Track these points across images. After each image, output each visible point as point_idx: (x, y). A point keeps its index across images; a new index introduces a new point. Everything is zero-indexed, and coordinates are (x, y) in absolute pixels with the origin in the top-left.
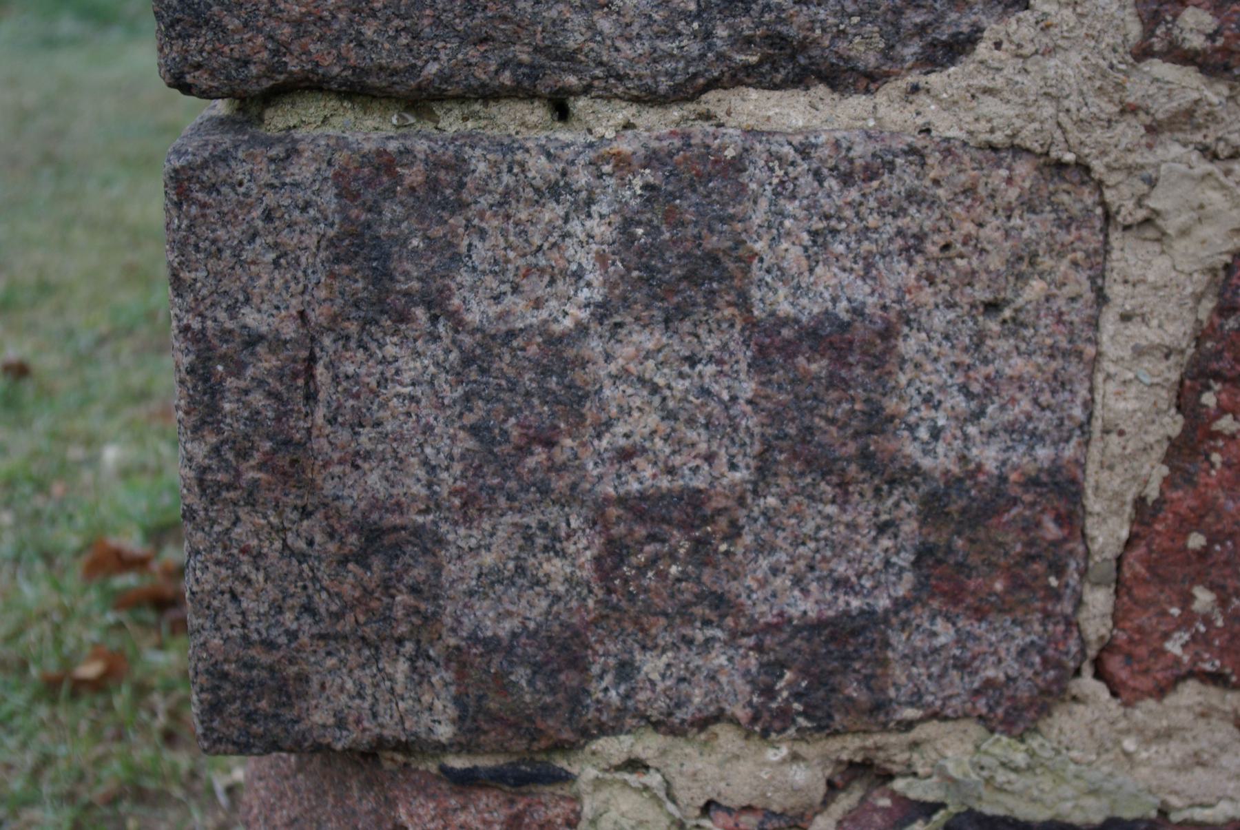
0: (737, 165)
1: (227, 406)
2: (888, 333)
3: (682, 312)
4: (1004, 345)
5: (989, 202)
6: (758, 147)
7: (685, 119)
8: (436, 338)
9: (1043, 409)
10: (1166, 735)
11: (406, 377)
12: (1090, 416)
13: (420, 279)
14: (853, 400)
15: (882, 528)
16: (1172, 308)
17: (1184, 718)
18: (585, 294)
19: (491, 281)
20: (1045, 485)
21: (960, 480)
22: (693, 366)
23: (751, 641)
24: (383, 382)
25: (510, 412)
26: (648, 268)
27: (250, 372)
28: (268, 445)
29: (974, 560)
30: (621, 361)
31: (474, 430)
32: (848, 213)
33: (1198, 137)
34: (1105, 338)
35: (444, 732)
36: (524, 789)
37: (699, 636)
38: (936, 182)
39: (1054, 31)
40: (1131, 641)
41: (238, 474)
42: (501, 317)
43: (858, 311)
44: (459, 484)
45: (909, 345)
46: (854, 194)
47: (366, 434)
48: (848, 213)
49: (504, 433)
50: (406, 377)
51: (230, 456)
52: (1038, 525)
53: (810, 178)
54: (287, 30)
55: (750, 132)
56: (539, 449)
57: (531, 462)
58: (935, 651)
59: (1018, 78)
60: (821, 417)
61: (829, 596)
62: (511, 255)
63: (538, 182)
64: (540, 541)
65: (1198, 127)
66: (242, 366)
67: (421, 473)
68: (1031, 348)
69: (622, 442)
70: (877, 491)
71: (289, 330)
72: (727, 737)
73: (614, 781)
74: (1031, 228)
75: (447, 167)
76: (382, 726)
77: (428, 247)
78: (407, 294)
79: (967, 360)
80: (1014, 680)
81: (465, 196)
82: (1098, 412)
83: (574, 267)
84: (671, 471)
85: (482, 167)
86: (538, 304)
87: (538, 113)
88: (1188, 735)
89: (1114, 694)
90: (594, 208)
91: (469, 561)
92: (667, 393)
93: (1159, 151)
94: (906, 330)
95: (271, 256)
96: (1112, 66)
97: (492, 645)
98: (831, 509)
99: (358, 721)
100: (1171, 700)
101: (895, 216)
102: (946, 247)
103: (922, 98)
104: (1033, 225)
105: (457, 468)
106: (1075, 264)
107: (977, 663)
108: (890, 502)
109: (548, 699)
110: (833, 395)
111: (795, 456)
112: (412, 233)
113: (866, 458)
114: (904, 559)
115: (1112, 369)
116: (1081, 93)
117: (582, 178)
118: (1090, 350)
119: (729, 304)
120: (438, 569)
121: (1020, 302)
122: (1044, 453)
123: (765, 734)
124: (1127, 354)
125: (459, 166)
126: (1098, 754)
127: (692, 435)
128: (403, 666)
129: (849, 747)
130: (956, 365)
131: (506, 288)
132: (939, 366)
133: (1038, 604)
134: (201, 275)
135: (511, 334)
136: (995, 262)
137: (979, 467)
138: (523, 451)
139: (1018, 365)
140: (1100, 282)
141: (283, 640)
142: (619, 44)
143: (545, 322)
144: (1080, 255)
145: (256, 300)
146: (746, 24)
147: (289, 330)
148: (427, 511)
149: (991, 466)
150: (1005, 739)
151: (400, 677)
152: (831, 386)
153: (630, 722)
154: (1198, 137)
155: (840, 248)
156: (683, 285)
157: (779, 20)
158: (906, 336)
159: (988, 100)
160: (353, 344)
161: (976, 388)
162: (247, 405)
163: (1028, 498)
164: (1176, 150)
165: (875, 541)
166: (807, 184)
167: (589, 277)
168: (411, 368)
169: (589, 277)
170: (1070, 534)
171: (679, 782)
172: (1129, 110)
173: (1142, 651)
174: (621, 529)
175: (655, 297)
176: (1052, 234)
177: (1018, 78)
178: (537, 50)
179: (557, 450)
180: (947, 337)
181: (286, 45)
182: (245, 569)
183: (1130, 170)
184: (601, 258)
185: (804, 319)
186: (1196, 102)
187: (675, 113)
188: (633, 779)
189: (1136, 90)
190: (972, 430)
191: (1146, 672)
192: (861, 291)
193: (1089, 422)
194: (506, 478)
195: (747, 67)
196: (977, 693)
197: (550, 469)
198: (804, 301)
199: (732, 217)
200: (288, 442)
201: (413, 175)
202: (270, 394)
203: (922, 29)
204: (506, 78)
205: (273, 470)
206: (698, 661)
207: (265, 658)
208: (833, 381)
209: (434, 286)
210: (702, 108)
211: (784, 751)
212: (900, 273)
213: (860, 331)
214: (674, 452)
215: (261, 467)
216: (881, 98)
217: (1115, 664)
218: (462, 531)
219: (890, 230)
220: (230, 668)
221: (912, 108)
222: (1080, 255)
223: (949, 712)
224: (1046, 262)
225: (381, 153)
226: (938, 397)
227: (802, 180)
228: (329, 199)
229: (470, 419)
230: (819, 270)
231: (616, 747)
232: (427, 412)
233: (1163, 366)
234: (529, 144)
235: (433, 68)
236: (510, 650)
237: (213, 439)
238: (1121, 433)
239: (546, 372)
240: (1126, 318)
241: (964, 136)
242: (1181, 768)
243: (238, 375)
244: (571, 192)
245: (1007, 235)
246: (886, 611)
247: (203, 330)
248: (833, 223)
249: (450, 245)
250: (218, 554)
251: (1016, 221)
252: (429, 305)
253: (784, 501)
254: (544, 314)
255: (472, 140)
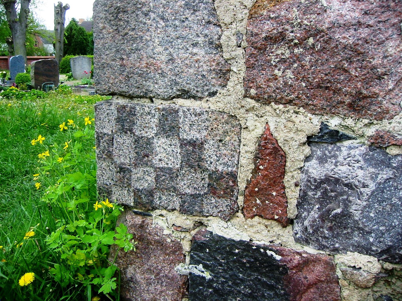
0: (177, 112)
1: (101, 144)
2: (202, 143)
3: (169, 136)
4: (223, 148)
5: (220, 121)
6: (181, 109)
7: (171, 103)
8: (131, 137)
9: (230, 161)
10: (252, 226)
11: (127, 143)
12: (238, 163)
13: (128, 126)
14: (196, 155)
15: (203, 179)
16: (251, 144)
17: (255, 223)
18: (154, 132)
19: (140, 128)
20: (229, 175)
21: (215, 172)
22: (171, 146)
23: (180, 196)
24: (123, 143)
25: (142, 150)
26: (163, 128)
27: (104, 139)
28: (107, 152)
29: (218, 187)
30: (159, 144)
31: (136, 153)
32: (196, 121)
33: (255, 113)
34: (241, 149)
35: (132, 204)
36: (145, 217)
37: (172, 194)
38: (210, 117)
39: (230, 91)
40: (247, 207)
41: (103, 156)
42: (141, 134)
43: (197, 139)
44: (134, 162)
45: (206, 146)
46: (197, 118)
47: (121, 151)
48: (196, 121)
49: (141, 154)
50: (127, 143)
51: (101, 152)
52: (229, 182)
53: (189, 114)
54: (110, 84)
55: (180, 106)
56: (146, 157)
57: (145, 159)
58: (211, 203)
59: (223, 100)
60: (191, 157)
61: (193, 190)
62: (143, 124)
63: (146, 112)
64: (146, 173)
65: (255, 111)
66: (103, 138)
67: (129, 159)
68: (228, 149)
69: (159, 158)
70: (201, 172)
71: (110, 133)
72: (176, 213)
73: (158, 218)
74: (227, 127)
75: (133, 108)
76: (123, 201)
77: (130, 121)
78: (127, 129)
79: (216, 150)
80: (225, 211)
81: (136, 113)
82: (240, 163)
83: (152, 127)
84: (167, 164)
85: (138, 109)
86: (147, 133)
87: (147, 100)
88: (256, 227)
89: (244, 216)
90: (155, 117)
91: (136, 175)
92: (166, 150)
93: (248, 115)
94: (206, 143)
95: (108, 121)
96: (239, 99)
97: (139, 190)
98: (194, 175)
99: (120, 200)
100: (253, 219)
101: (204, 123)
102: (212, 129)
103: (209, 102)
104: (227, 126)
105: (134, 159)
106: (235, 134)
107: (219, 207)
108: (204, 174)
109: (147, 201)
110: (193, 154)
111: (187, 164)
112: (127, 119)
113: (199, 166)
114: (206, 185)
115: (242, 155)
116: (234, 103)
117: (153, 112)
118: (238, 151)
119: (176, 136)
120: (131, 176)
121: (225, 140)
122: (230, 169)
123: (182, 213)
124: (244, 152)
125: (134, 108)
126: (240, 227)
127: (171, 158)
128: (126, 192)
129: (197, 218)
130: (215, 151)
131: (142, 129)
132: (212, 150)
133: (229, 197)
134: (98, 123)
135: (142, 137)
136: (220, 132)
137: (218, 170)
138: (144, 157)
139: (225, 152)
140: (240, 138)
141: (109, 184)
142: (158, 89)
143: (147, 136)
144: (235, 133)
145: (106, 128)
146: (178, 88)
147: (110, 133)
148: (129, 166)
149: (220, 170)
150: (223, 222)
151: (126, 193)
152: (192, 152)
153: (161, 208)
154: (255, 113)
155: (195, 128)
156: (169, 131)
157: (183, 87)
158: (206, 144)
159: (218, 103)
160: (119, 136)
161: (218, 155)
162: (104, 145)
163: (227, 177)
164: (251, 115)
165: (201, 181)
166: (189, 116)
167: (154, 129)
168: (128, 141)
169: (154, 129)
170: (235, 185)
171: (169, 220)
172: (242, 107)
173: (249, 209)
174: (159, 173)
175: (164, 133)
176: (231, 128)
177: (223, 100)
178: (146, 90)
179: (149, 158)
180: (213, 145)
181: (110, 87)
182: (103, 172)
183: (244, 118)
184: (156, 125)
185: (188, 139)
186: (254, 106)
187: (169, 102)
188: (161, 218)
189: (243, 103)
190: (217, 163)
191: (249, 213)
192: (198, 136)
193: (238, 164)
194: (141, 162)
195: (179, 95)
196: (219, 212)
197: (148, 161)
198: (188, 136)
199: (176, 120)
200: (109, 151)
201: (128, 109)
202: (107, 143)
203: (208, 90)
204: (142, 94)
205: (107, 156)
206: (171, 199)
207: (106, 187)
208: (193, 151)
209: (131, 128)
210: (173, 101)
211: (185, 217)
212: (205, 133)
213: (198, 142)
214: (168, 161)
215: (105, 155)
216: (202, 102)
217: (245, 211)
218: (135, 170)
219: (203, 125)
220: (101, 187)
221: (207, 104)
222: (235, 133)
223: (214, 215)
224: (230, 133)
225: (123, 105)
226: (212, 156)
227: (188, 115)
228: (116, 112)
229: (136, 151)
230: (191, 131)
231: (158, 212)
232: (130, 150)
233: (250, 155)
234: (146, 106)
235: (131, 92)
236: (141, 191)
237: (99, 150)
238: (243, 167)
239: (147, 144)
240: (244, 145)
241: (215, 109)
242: (255, 233)
243: (102, 139)
244: (151, 114)
245: (222, 128)
246: (203, 194)
247: (98, 132)
248: (193, 123)
249: (133, 121)
250: (100, 168)
251: (224, 125)
252: (130, 131)
253: (186, 172)
254: (147, 134)
255: (138, 104)
